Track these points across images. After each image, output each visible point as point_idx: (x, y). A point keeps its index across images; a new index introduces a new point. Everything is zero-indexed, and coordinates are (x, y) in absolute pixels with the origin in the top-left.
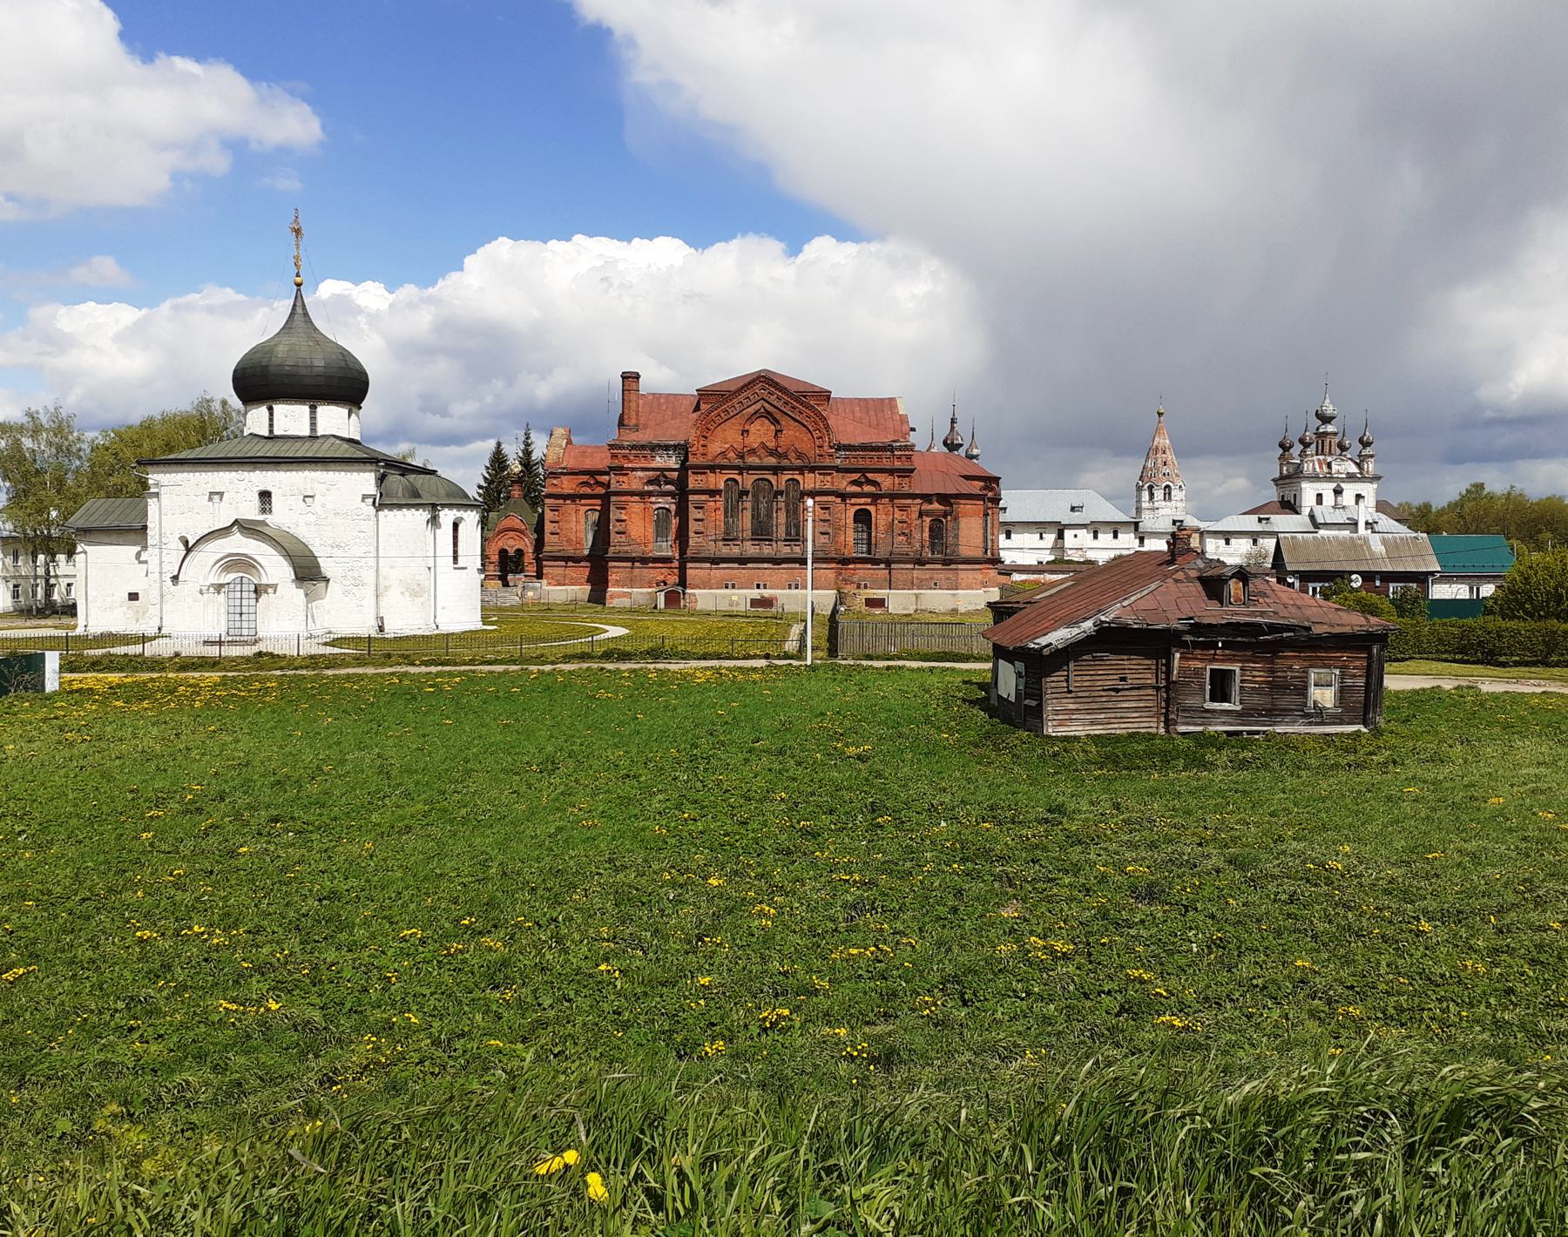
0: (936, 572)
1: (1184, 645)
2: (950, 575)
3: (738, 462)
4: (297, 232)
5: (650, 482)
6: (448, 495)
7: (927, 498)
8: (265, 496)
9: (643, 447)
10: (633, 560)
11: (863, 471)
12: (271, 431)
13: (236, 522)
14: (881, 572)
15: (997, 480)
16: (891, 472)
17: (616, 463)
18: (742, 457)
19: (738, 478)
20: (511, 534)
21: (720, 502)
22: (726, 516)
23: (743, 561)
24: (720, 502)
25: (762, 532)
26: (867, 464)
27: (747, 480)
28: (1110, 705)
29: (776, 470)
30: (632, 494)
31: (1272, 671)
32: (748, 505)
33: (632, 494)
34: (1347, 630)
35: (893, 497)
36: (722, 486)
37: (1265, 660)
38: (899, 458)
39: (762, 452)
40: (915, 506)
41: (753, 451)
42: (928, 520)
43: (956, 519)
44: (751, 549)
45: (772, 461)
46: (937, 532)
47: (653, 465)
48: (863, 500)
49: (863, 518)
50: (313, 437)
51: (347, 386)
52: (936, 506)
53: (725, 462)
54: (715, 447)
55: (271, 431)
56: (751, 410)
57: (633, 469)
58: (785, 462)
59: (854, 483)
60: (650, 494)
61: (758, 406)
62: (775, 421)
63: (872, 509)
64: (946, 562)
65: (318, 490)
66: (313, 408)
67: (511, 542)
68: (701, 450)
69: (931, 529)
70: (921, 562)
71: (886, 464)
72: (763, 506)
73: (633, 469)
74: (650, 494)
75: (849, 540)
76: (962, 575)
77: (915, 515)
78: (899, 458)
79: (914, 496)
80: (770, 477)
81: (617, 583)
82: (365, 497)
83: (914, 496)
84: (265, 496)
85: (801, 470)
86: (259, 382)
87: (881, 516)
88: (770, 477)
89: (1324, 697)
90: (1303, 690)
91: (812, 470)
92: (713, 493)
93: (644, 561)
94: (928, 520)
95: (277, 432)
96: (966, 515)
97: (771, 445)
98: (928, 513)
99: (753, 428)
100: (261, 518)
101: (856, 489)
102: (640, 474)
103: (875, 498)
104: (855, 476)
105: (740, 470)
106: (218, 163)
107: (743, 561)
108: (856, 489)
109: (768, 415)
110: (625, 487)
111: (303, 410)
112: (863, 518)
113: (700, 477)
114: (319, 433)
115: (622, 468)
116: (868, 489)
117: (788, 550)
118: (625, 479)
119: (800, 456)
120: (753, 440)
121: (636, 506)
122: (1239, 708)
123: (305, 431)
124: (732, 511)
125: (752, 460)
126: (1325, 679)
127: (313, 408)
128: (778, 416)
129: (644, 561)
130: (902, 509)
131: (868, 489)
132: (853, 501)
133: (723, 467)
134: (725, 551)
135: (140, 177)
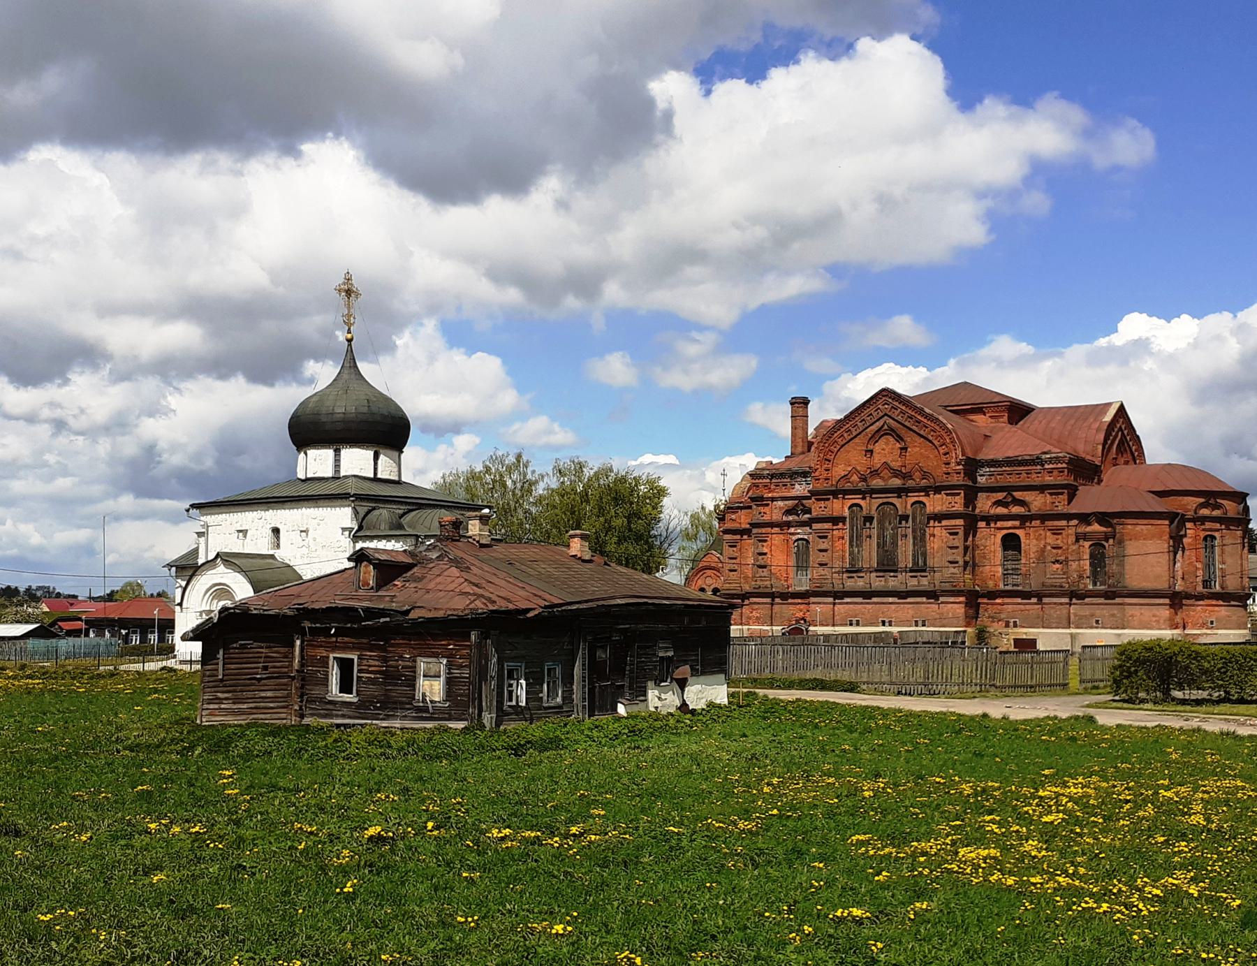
0: (1104, 610)
1: (302, 633)
2: (1115, 610)
3: (862, 485)
4: (349, 292)
5: (788, 512)
6: (391, 529)
7: (1084, 518)
8: (276, 531)
9: (782, 475)
10: (772, 596)
11: (1009, 489)
12: (375, 474)
13: (218, 555)
14: (1032, 606)
15: (1240, 497)
16: (1041, 489)
17: (758, 493)
18: (864, 479)
19: (862, 502)
20: (709, 572)
21: (845, 530)
22: (851, 545)
23: (867, 595)
24: (845, 530)
25: (887, 565)
26: (1012, 480)
27: (870, 505)
28: (250, 694)
29: (900, 492)
30: (771, 525)
31: (385, 660)
32: (875, 532)
33: (771, 525)
34: (440, 614)
35: (1044, 517)
36: (846, 513)
37: (378, 648)
38: (1050, 472)
39: (886, 473)
40: (1073, 527)
41: (875, 473)
42: (1087, 544)
43: (1121, 542)
44: (877, 583)
45: (896, 482)
46: (1098, 559)
47: (793, 493)
48: (1010, 524)
49: (1011, 543)
50: (336, 478)
51: (388, 431)
52: (1096, 527)
53: (848, 486)
54: (840, 470)
55: (375, 474)
56: (875, 427)
57: (773, 499)
58: (910, 483)
59: (998, 503)
60: (788, 525)
61: (879, 424)
62: (899, 438)
63: (1020, 532)
64: (1109, 595)
65: (312, 525)
66: (337, 452)
67: (709, 581)
68: (825, 474)
69: (1092, 556)
70: (1076, 595)
71: (1036, 480)
72: (889, 532)
73: (773, 499)
74: (788, 525)
75: (993, 568)
76: (1130, 611)
77: (1072, 539)
78: (1050, 472)
79: (1069, 517)
80: (894, 501)
81: (736, 624)
82: (344, 529)
83: (1069, 517)
84: (276, 531)
85: (926, 490)
86: (308, 430)
87: (1031, 540)
88: (894, 501)
89: (432, 689)
90: (412, 682)
91: (938, 490)
92: (836, 520)
93: (785, 596)
94: (1087, 544)
95: (379, 476)
96: (1136, 537)
97: (895, 465)
98: (1085, 537)
99: (877, 448)
100: (271, 552)
101: (1001, 510)
102: (780, 503)
103: (1024, 519)
104: (1000, 496)
105: (863, 493)
106: (1037, 202)
107: (867, 595)
108: (1001, 510)
109: (892, 432)
110: (767, 518)
111: (328, 453)
112: (1011, 543)
113: (822, 504)
114: (343, 473)
115: (762, 498)
116: (1016, 510)
117: (914, 582)
118: (767, 509)
119: (925, 475)
120: (878, 461)
121: (777, 538)
122: (355, 700)
123: (328, 472)
124: (856, 540)
125: (877, 483)
126: (434, 669)
127: (337, 452)
128: (903, 432)
129: (785, 596)
130: (1056, 532)
131: (1016, 510)
132: (999, 524)
133: (846, 492)
134: (850, 584)
135: (962, 226)
